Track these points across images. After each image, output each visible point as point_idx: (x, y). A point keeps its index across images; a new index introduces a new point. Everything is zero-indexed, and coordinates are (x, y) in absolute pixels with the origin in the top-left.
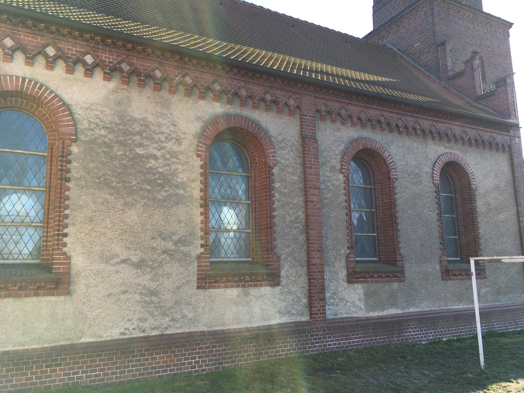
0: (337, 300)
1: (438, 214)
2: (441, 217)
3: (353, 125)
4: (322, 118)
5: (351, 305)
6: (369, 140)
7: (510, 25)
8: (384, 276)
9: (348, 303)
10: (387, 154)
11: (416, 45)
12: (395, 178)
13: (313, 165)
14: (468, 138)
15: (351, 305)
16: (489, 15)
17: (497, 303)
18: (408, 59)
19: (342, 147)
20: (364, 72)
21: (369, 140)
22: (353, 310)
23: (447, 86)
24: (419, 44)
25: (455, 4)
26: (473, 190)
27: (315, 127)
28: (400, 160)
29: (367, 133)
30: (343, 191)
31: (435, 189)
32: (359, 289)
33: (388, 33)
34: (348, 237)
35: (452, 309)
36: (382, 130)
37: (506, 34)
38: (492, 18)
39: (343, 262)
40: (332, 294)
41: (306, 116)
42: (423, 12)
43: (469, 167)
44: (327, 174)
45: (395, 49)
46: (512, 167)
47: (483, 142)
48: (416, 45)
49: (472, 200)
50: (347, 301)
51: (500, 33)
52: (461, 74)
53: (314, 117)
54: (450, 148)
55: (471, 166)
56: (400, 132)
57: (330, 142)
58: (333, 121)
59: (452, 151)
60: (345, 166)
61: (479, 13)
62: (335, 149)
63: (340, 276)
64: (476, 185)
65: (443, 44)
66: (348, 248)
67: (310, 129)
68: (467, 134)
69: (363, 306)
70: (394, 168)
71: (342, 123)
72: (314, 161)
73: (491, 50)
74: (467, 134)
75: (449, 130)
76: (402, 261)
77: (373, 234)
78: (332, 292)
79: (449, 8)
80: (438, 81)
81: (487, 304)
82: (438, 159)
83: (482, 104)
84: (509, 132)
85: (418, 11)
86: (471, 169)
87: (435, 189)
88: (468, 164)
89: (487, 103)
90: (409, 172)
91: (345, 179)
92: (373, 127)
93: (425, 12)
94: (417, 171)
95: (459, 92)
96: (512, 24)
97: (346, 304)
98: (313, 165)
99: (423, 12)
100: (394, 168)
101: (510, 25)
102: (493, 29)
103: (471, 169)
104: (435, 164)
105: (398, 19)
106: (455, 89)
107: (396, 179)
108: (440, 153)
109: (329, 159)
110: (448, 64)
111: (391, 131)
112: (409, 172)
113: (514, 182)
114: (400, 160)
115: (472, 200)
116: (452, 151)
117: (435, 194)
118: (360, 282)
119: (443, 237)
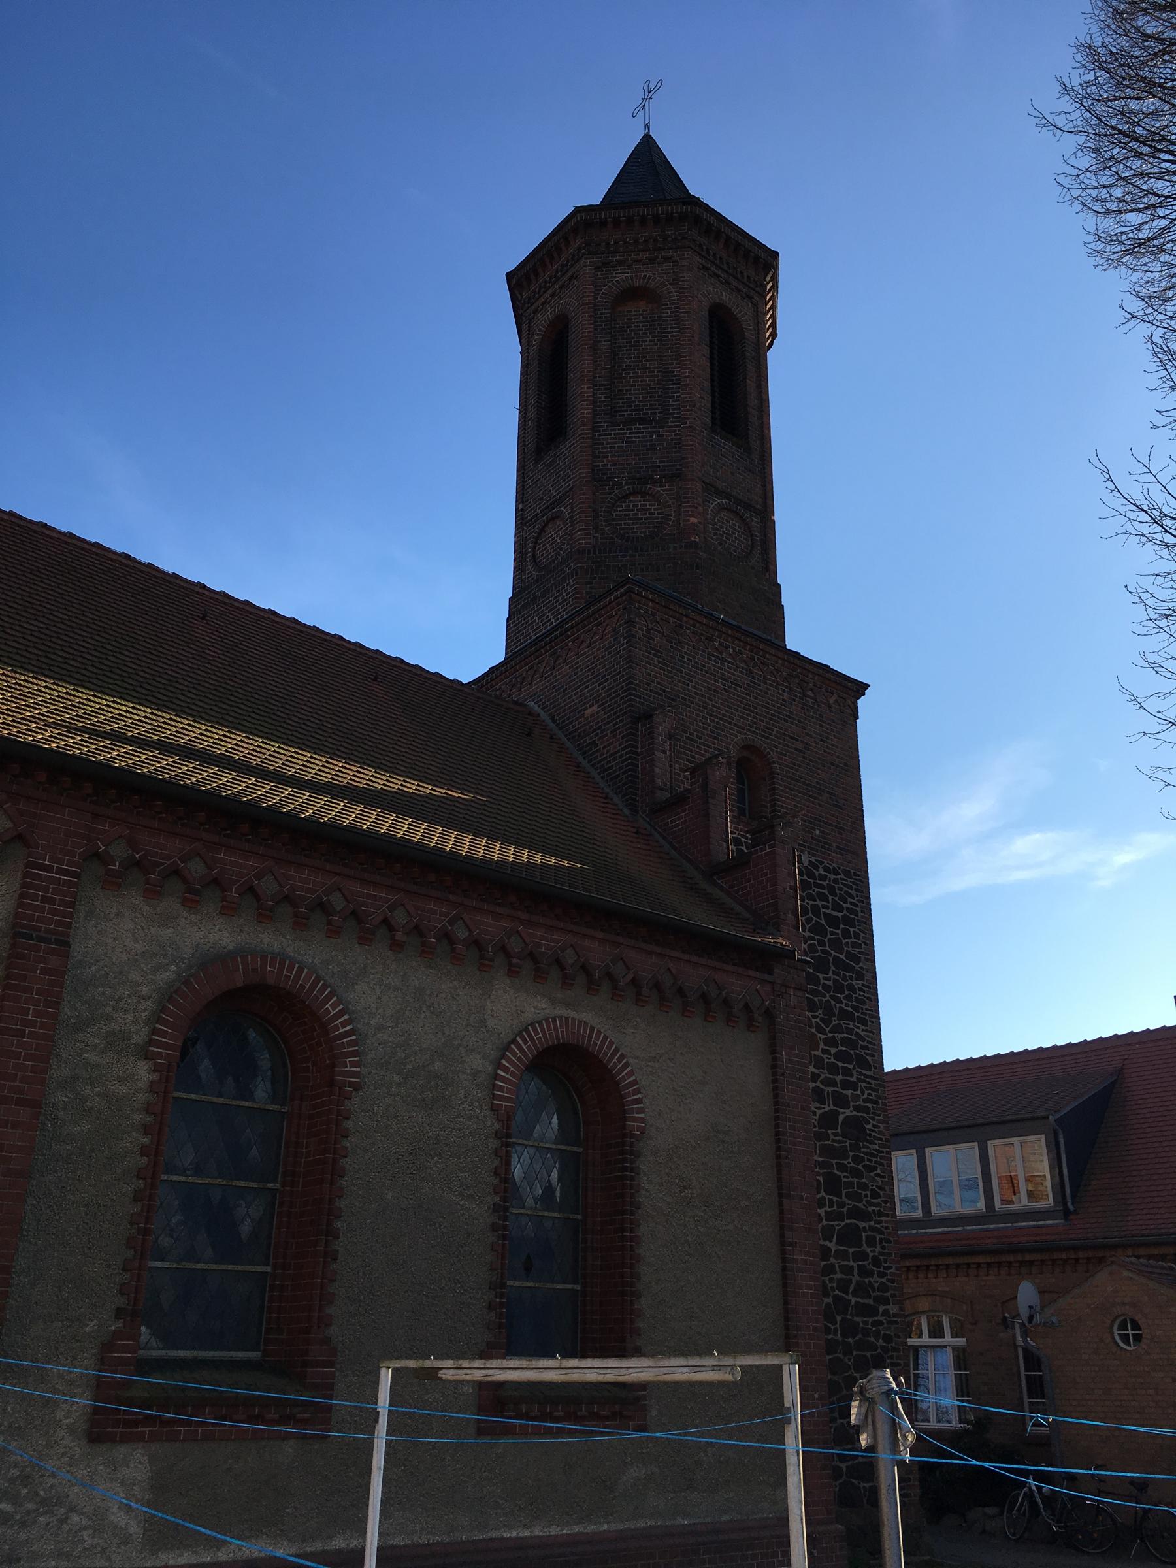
0: (30, 1506)
1: (496, 1208)
2: (505, 1219)
3: (228, 910)
4: (113, 882)
5: (85, 1521)
6: (273, 959)
7: (860, 688)
8: (584, 1412)
9: (75, 1518)
10: (334, 1006)
11: (588, 712)
12: (351, 1084)
13: (31, 1024)
14: (630, 976)
15: (85, 1521)
16: (797, 655)
17: (680, 1521)
18: (569, 744)
19: (168, 975)
20: (365, 762)
21: (273, 959)
22: (88, 1542)
23: (649, 827)
24: (595, 708)
25: (698, 618)
26: (633, 1136)
27: (72, 905)
28: (380, 1028)
29: (273, 939)
30: (138, 1118)
31: (497, 1126)
32: (136, 1462)
33: (532, 671)
34: (126, 1276)
35: (502, 1539)
36: (334, 932)
37: (848, 711)
38: (807, 666)
39: (84, 1369)
40: (12, 1481)
41: (48, 869)
42: (609, 629)
43: (626, 1065)
44: (92, 1057)
45: (544, 715)
46: (774, 1074)
47: (680, 991)
48: (588, 712)
49: (625, 1169)
50: (72, 1509)
51: (829, 706)
52: (679, 800)
53: (77, 875)
54: (568, 1005)
55: (631, 1061)
56: (396, 946)
57: (124, 957)
58: (153, 893)
59: (573, 1014)
60: (163, 1034)
61: (768, 649)
62: (139, 979)
63: (60, 1415)
64: (642, 1120)
65: (648, 716)
66: (119, 1313)
67: (53, 912)
68: (628, 969)
69: (135, 1529)
70: (355, 1054)
71: (185, 902)
72: (37, 1013)
73: (799, 746)
74: (628, 969)
75: (569, 951)
76: (331, 1364)
77: (259, 1269)
78: (15, 1472)
79: (681, 626)
80: (626, 811)
81: (641, 1524)
82: (520, 1034)
83: (722, 889)
84: (770, 972)
85: (600, 624)
86: (631, 1073)
87: (497, 1126)
88: (623, 1056)
89: (731, 887)
90: (409, 1067)
91: (155, 1077)
92: (300, 923)
93: (614, 629)
94: (437, 1066)
95: (675, 849)
96: (867, 686)
97: (63, 1521)
98: (31, 1024)
99: (609, 629)
100: (355, 1054)
101: (860, 688)
102: (810, 693)
103: (631, 1073)
104: (507, 1048)
105: (557, 637)
106: (665, 838)
107: (357, 1088)
108: (530, 1014)
109: (109, 1009)
110: (657, 770)
111: (365, 939)
112: (409, 1067)
113: (777, 1118)
114: (380, 1028)
115: (625, 1169)
116: (573, 1014)
117: (494, 1143)
118: (140, 1438)
119: (503, 1285)
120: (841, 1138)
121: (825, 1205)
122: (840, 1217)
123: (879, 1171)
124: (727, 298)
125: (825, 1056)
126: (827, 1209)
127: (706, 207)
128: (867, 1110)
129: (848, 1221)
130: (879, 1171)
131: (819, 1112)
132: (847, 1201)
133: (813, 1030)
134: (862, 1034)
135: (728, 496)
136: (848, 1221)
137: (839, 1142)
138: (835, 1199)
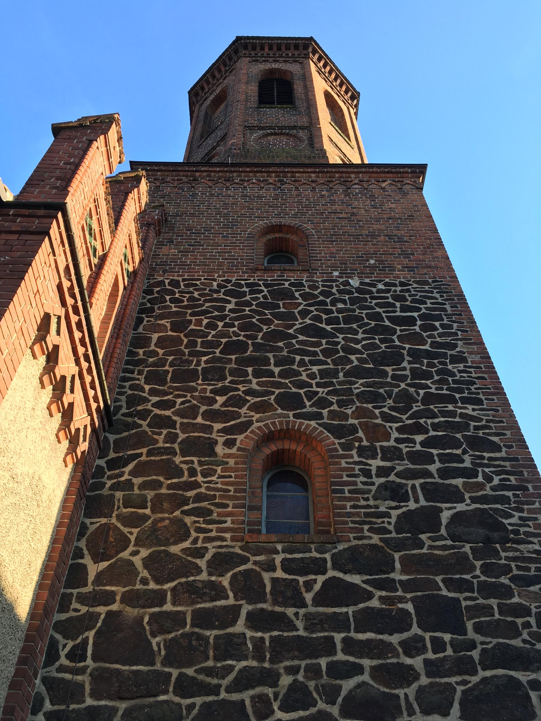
7: (419, 170)
96: (427, 165)
120: (449, 542)
121: (424, 649)
122: (465, 667)
123: (215, 284)
124: (338, 380)
125: (402, 446)
126: (430, 655)
127: (248, 38)
128: (505, 500)
129: (488, 673)
130: (215, 284)
131: (395, 513)
132: (479, 638)
133: (379, 421)
134: (475, 413)
135: (261, 128)
136: (488, 673)
137: (444, 548)
138: (447, 637)
